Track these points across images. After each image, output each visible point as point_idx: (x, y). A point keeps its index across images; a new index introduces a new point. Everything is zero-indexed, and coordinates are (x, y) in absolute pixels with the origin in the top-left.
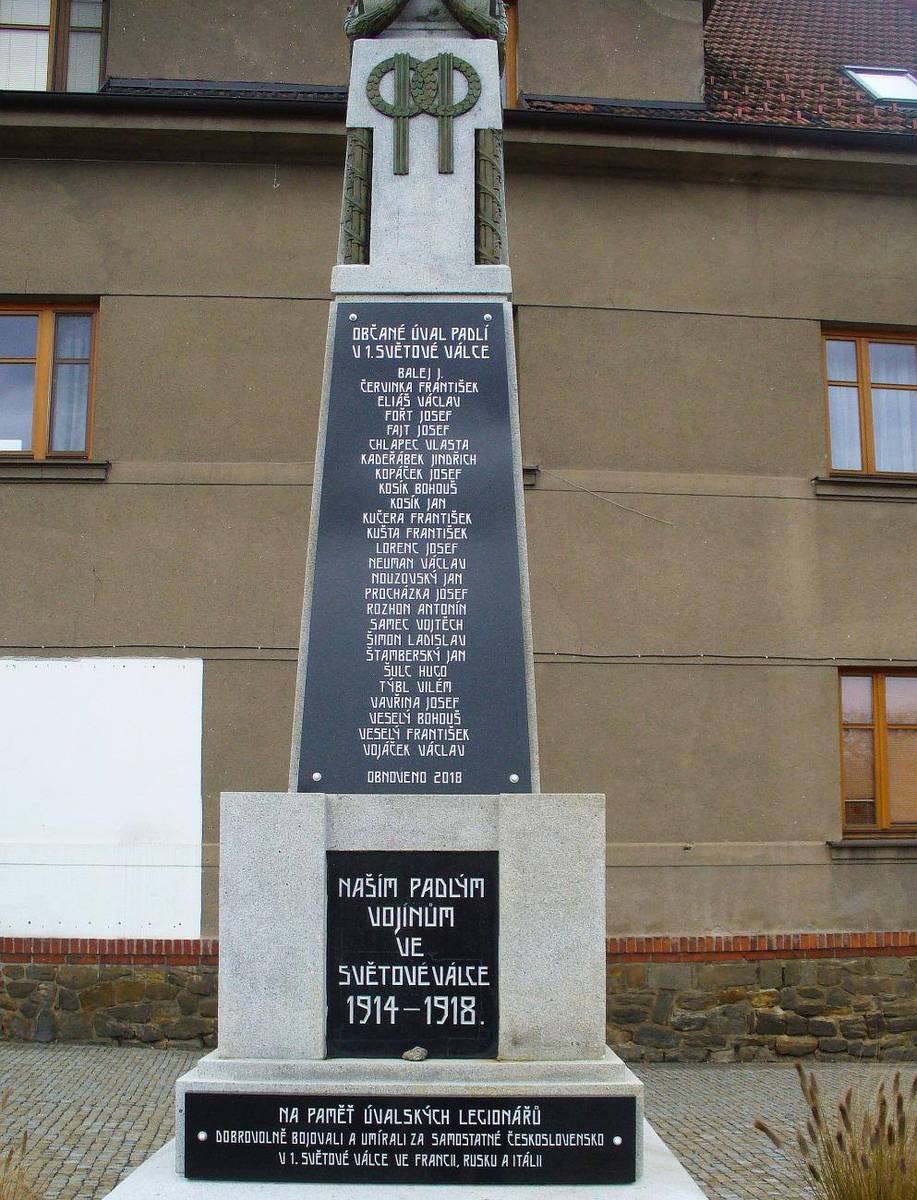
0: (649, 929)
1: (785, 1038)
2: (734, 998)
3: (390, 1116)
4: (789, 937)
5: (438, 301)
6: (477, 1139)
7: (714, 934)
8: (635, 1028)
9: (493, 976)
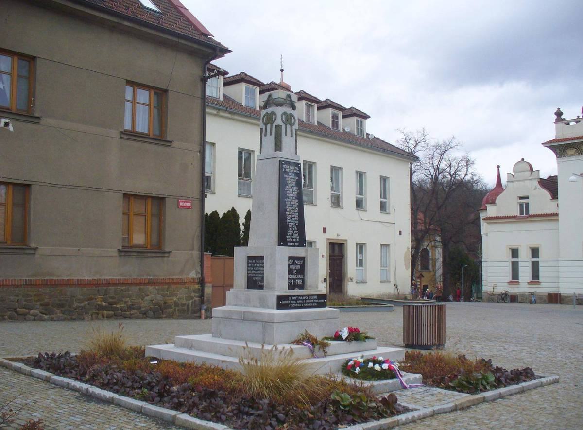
0: (68, 276)
2: (91, 299)
3: (301, 298)
4: (107, 279)
6: (310, 301)
8: (63, 309)
9: (304, 277)
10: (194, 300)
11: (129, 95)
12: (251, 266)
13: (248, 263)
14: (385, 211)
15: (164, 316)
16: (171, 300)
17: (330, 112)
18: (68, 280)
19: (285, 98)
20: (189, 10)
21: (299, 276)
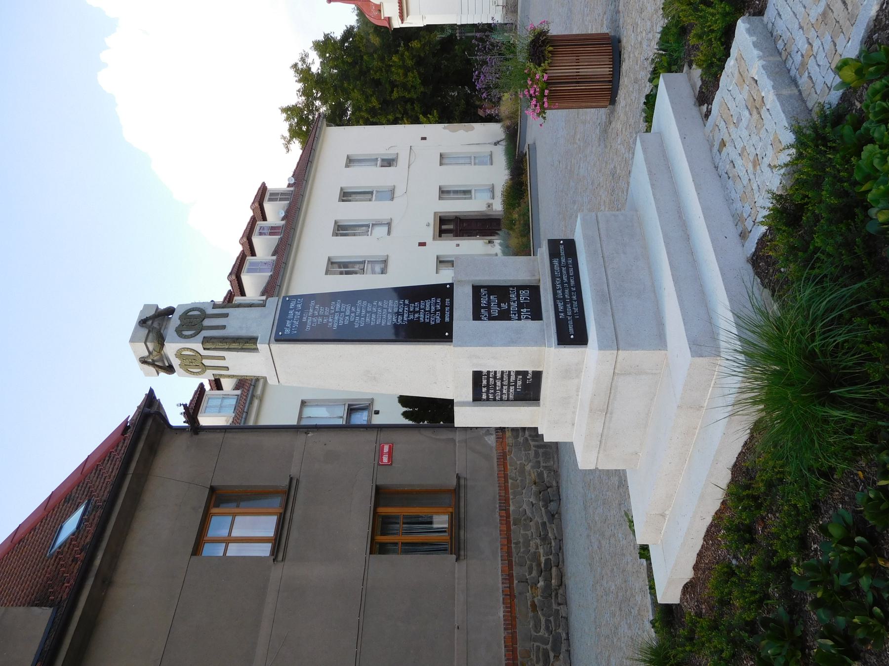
1: (553, 581)
3: (559, 292)
4: (503, 579)
5: (278, 318)
6: (564, 272)
7: (501, 614)
9: (513, 287)
10: (529, 438)
11: (217, 550)
12: (494, 394)
13: (488, 399)
14: (393, 160)
15: (554, 484)
16: (530, 475)
17: (256, 240)
18: (505, 647)
19: (146, 331)
20: (89, 454)
21: (513, 296)
